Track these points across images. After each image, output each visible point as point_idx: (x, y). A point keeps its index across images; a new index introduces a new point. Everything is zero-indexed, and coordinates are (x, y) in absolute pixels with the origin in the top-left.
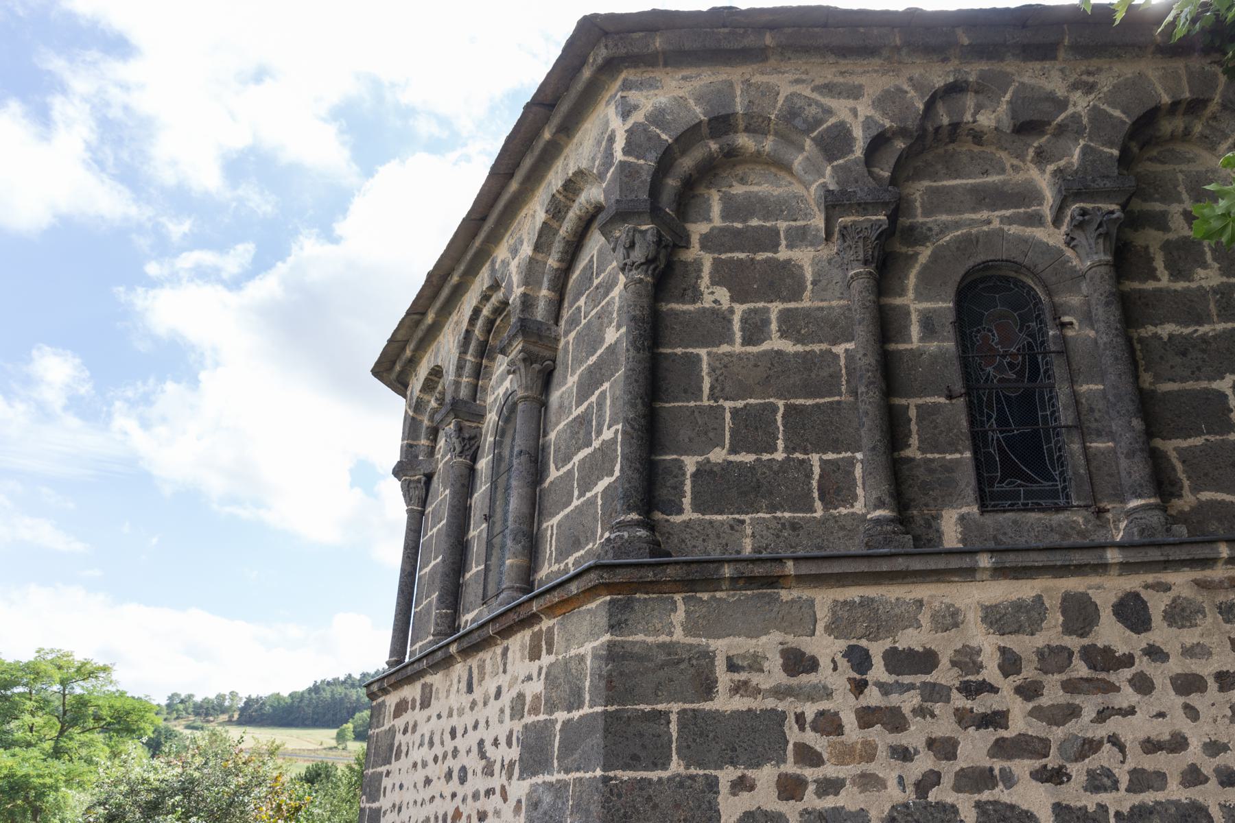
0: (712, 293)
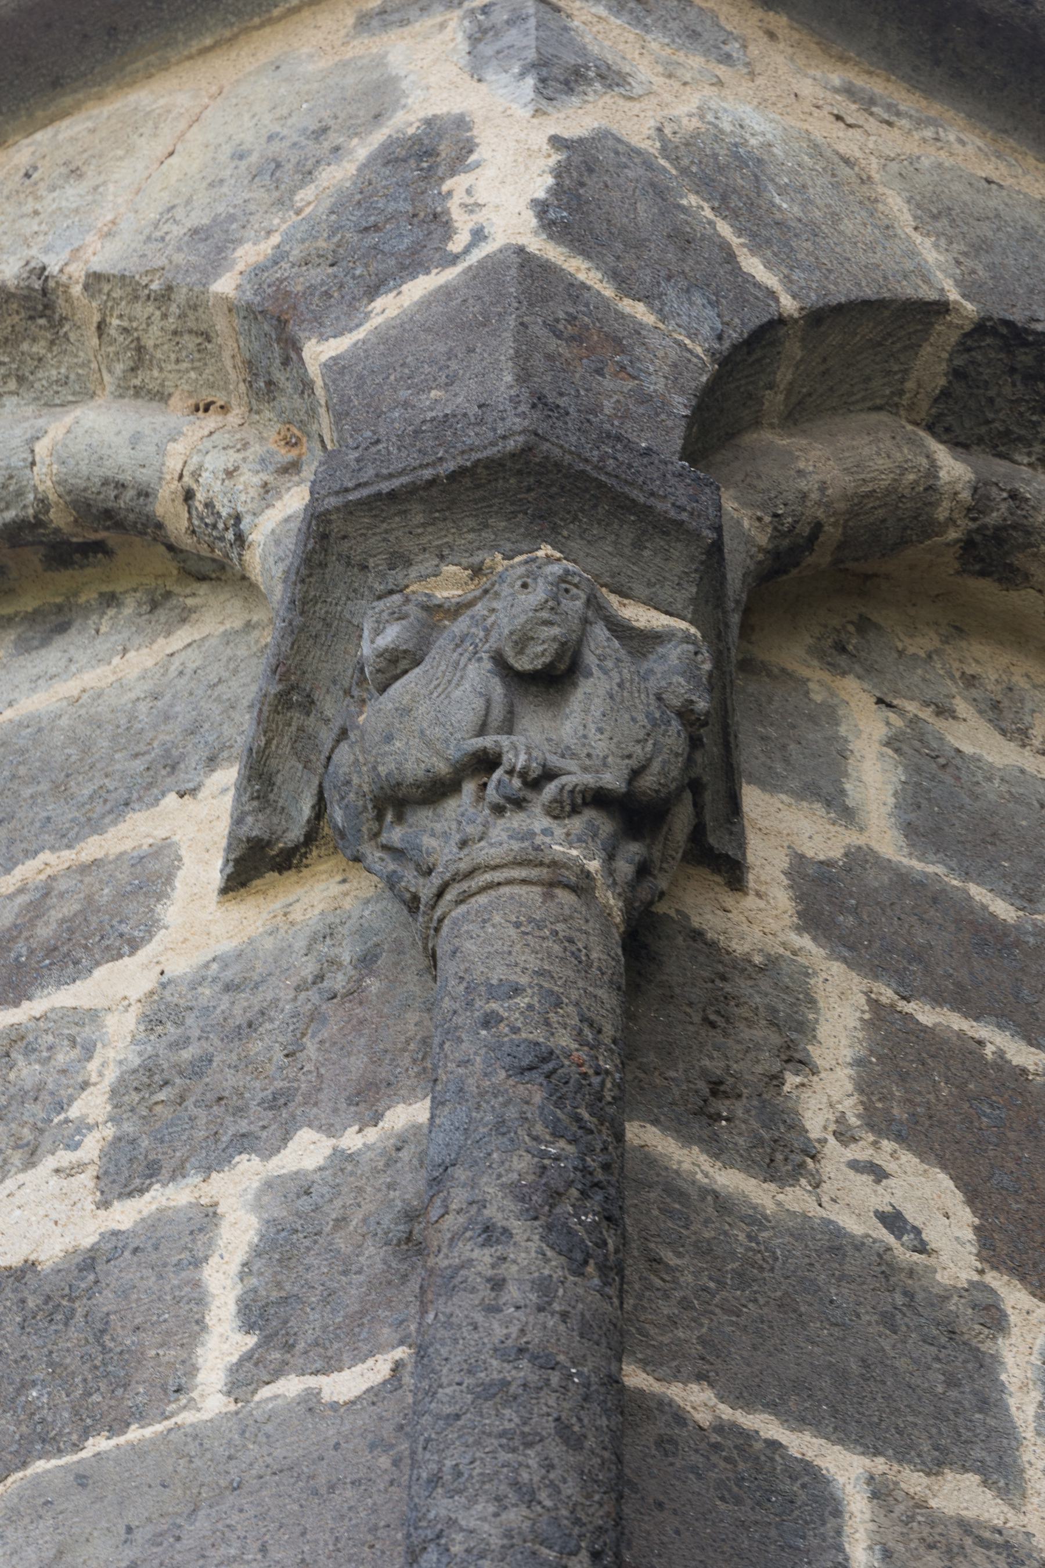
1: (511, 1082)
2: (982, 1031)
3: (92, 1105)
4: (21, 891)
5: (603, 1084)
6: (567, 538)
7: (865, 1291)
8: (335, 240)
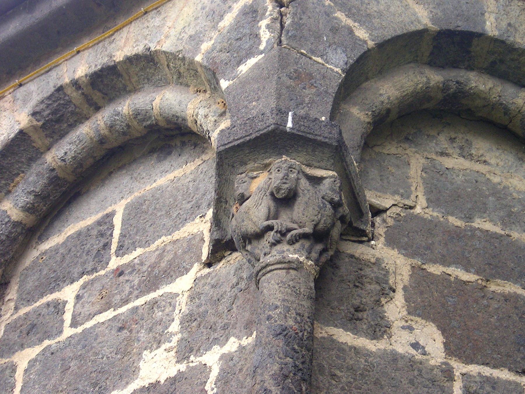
0: (411, 329)
1: (274, 339)
2: (450, 270)
3: (175, 327)
4: (157, 250)
5: (303, 335)
6: (291, 153)
7: (404, 373)
8: (229, 42)
